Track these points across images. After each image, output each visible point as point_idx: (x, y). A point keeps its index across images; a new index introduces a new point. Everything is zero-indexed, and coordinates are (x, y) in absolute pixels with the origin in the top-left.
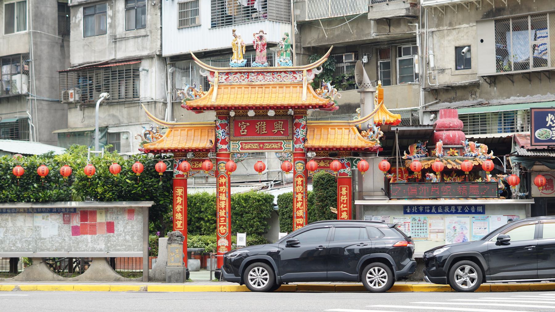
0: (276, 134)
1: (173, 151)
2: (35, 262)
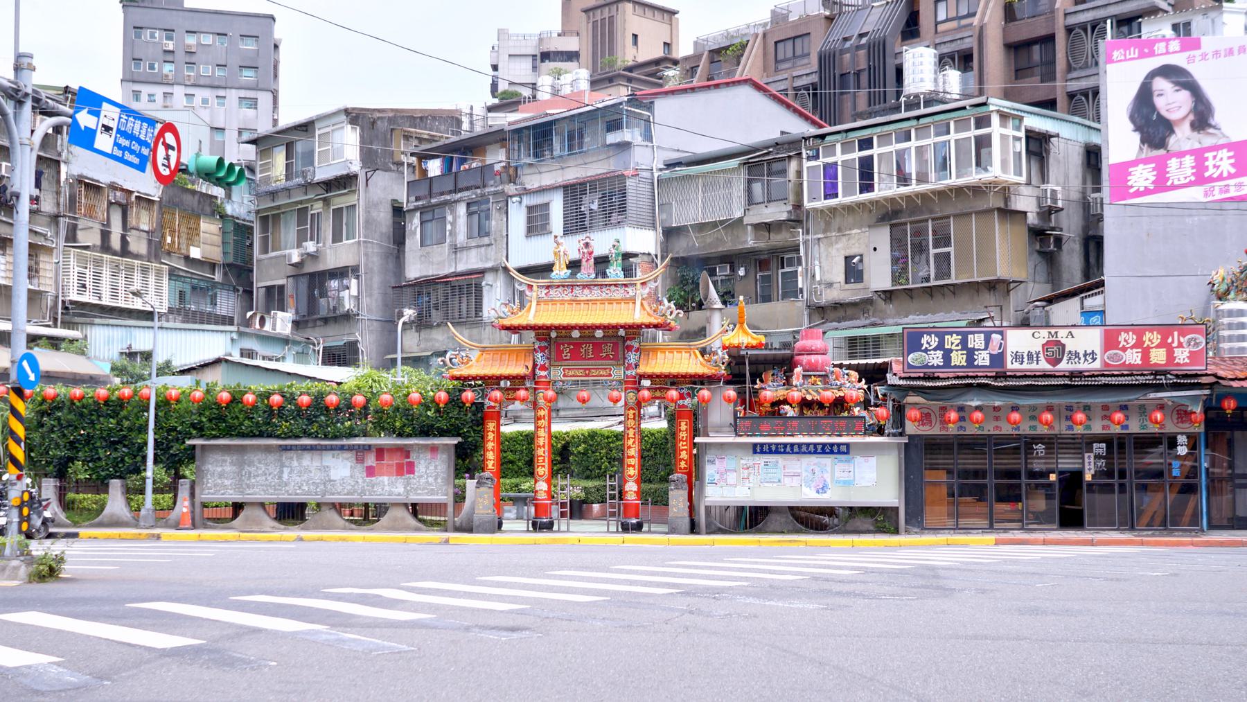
0: (604, 359)
1: (482, 378)
2: (323, 508)
